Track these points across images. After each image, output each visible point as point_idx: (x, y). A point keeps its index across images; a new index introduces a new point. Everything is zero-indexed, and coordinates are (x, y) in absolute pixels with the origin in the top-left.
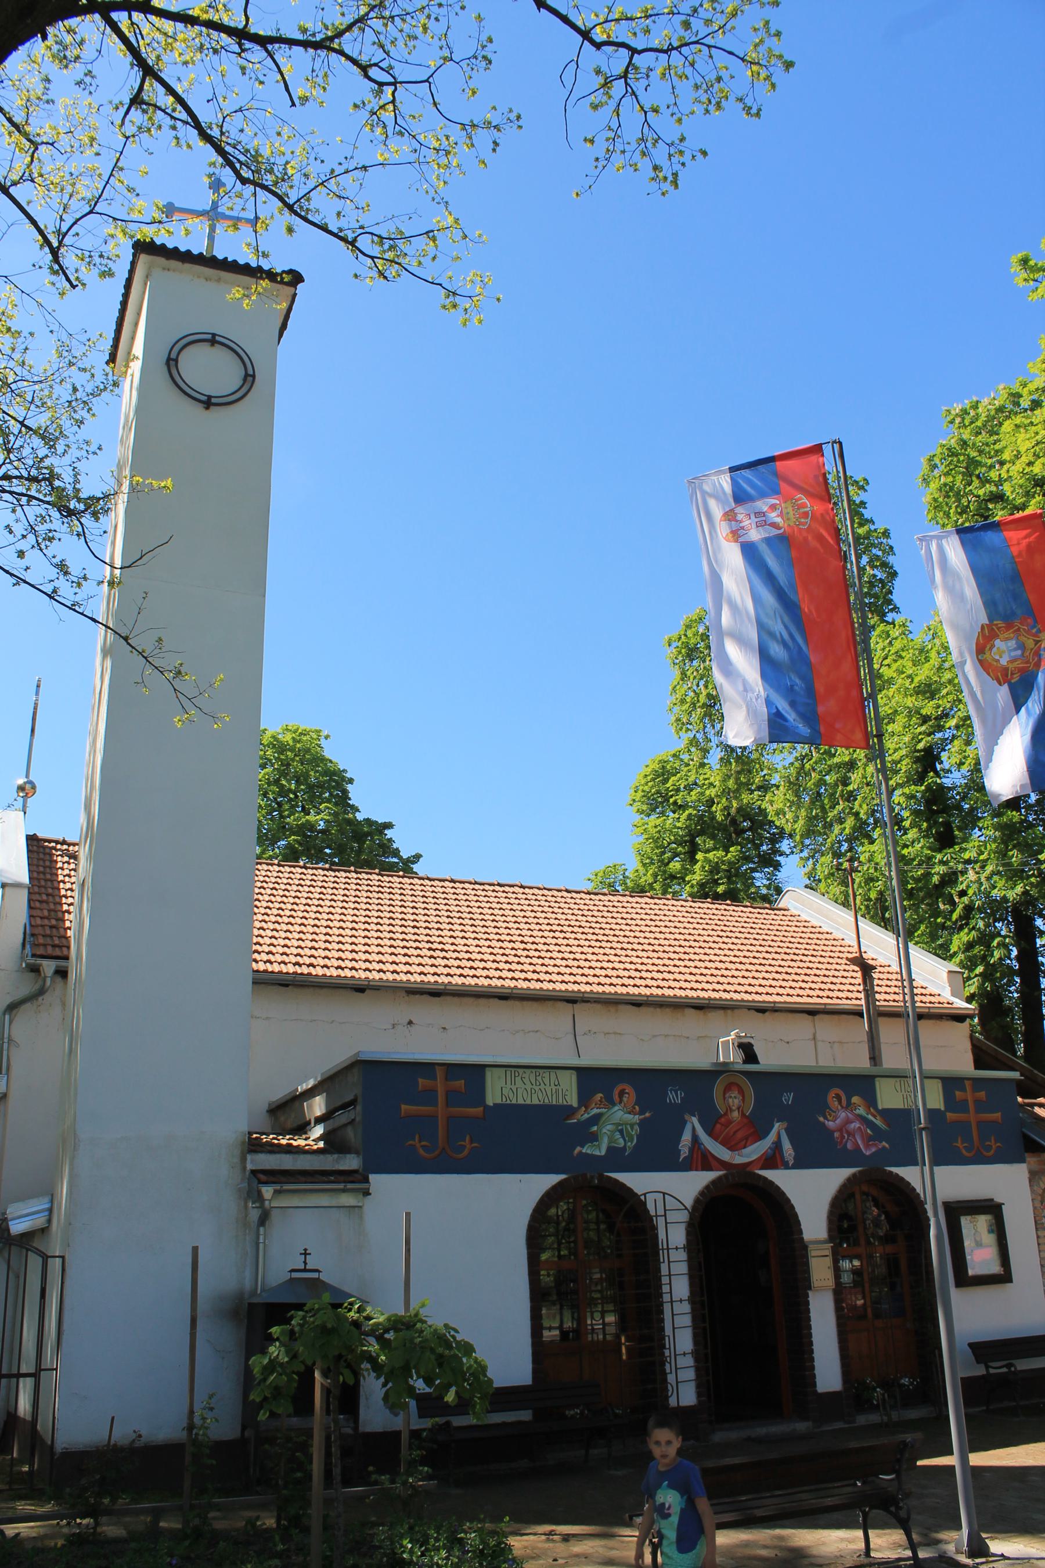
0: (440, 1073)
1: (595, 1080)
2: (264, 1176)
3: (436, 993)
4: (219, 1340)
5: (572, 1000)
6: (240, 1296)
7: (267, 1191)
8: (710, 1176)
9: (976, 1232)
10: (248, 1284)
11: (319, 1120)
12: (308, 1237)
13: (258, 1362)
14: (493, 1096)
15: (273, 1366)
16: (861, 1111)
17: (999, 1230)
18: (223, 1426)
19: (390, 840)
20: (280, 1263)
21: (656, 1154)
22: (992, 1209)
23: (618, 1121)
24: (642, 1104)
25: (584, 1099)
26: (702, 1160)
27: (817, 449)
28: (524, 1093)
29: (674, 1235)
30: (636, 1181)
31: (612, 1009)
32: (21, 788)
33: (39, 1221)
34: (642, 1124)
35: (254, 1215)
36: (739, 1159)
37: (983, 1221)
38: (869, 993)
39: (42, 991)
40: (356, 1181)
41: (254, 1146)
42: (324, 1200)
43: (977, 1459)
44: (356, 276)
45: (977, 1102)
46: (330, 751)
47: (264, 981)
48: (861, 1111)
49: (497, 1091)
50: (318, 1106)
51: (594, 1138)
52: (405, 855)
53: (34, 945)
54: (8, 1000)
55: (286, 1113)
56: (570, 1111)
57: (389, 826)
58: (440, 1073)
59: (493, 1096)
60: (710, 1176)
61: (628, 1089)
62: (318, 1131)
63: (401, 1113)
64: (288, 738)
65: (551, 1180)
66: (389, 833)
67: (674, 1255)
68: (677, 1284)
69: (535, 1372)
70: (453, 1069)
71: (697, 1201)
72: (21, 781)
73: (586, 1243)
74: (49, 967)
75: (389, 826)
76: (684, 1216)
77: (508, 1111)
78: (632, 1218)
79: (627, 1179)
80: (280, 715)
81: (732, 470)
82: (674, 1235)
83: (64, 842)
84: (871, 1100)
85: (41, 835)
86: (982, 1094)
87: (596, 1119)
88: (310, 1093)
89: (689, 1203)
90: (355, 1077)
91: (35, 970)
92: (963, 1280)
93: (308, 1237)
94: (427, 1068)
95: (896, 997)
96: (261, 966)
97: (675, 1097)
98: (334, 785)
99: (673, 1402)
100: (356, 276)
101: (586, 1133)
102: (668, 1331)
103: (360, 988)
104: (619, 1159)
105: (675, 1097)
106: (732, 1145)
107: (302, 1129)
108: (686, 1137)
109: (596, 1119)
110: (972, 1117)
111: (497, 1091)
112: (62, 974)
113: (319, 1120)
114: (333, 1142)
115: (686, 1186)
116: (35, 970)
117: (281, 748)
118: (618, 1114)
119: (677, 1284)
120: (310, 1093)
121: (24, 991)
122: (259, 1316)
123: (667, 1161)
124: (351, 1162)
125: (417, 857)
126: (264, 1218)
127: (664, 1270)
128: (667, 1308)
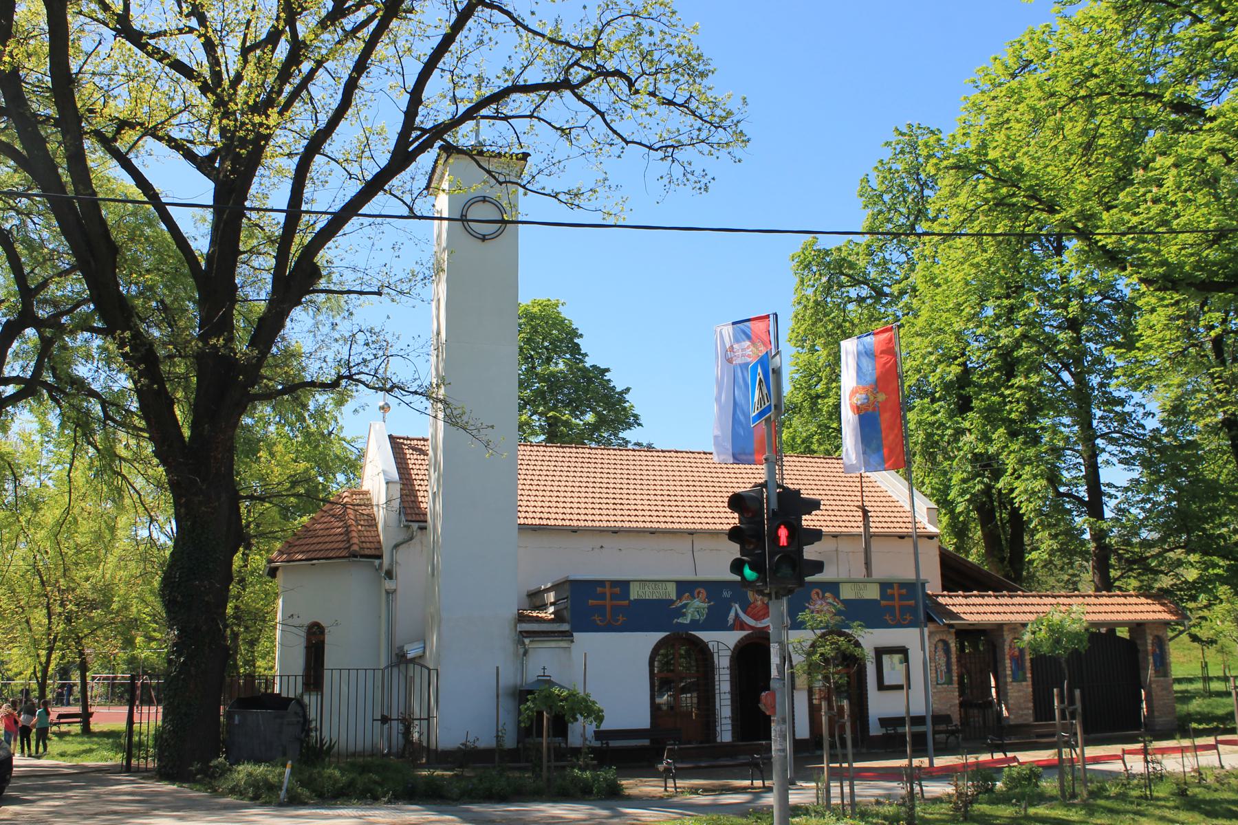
0: (607, 585)
1: (684, 587)
2: (528, 632)
3: (616, 532)
4: (507, 704)
5: (692, 533)
6: (515, 687)
7: (527, 641)
8: (744, 633)
9: (892, 665)
10: (519, 682)
11: (552, 604)
12: (546, 661)
13: (523, 707)
14: (633, 595)
15: (528, 708)
16: (830, 600)
17: (906, 660)
18: (510, 742)
19: (609, 380)
20: (533, 673)
21: (717, 621)
22: (903, 651)
23: (697, 607)
24: (709, 598)
25: (679, 596)
26: (740, 625)
27: (768, 316)
28: (649, 594)
29: (723, 662)
30: (704, 636)
31: (232, 814)
32: (382, 408)
33: (419, 652)
34: (709, 608)
35: (521, 651)
36: (760, 625)
37: (897, 658)
38: (867, 526)
39: (411, 539)
40: (567, 635)
41: (521, 618)
42: (553, 644)
43: (855, 765)
44: (585, 7)
45: (900, 595)
46: (565, 313)
47: (523, 527)
48: (830, 600)
49: (635, 593)
50: (551, 597)
51: (684, 615)
52: (618, 389)
53: (406, 514)
54: (394, 543)
55: (535, 598)
56: (672, 602)
57: (607, 370)
58: (607, 585)
59: (633, 595)
60: (744, 633)
61: (702, 590)
62: (552, 609)
63: (591, 605)
64: (536, 309)
65: (661, 635)
66: (608, 376)
67: (722, 671)
68: (724, 685)
69: (651, 723)
70: (615, 583)
71: (736, 646)
72: (382, 404)
73: (681, 663)
74: (415, 526)
75: (607, 370)
76: (729, 653)
77: (640, 602)
78: (703, 654)
79: (702, 635)
80: (529, 294)
81: (734, 323)
82: (723, 662)
83: (408, 439)
84: (836, 594)
85: (395, 434)
86: (904, 591)
87: (685, 606)
88: (547, 590)
89: (732, 647)
90: (567, 586)
91: (408, 527)
92: (881, 686)
93: (546, 661)
94: (601, 583)
95: (909, 525)
96: (522, 521)
97: (726, 594)
98: (566, 340)
99: (719, 740)
100: (585, 7)
101: (680, 612)
102: (718, 706)
103: (575, 530)
104: (696, 625)
105: (726, 594)
106: (756, 618)
107: (543, 607)
108: (732, 614)
109: (685, 606)
110: (896, 603)
111: (635, 593)
112: (423, 529)
113: (552, 604)
114: (558, 617)
115: (731, 638)
116: (408, 527)
117: (530, 317)
118: (697, 603)
119: (724, 685)
120: (547, 590)
121: (400, 539)
122: (521, 695)
123: (721, 625)
124: (565, 627)
125: (628, 390)
126: (525, 653)
127: (717, 678)
128: (717, 696)
